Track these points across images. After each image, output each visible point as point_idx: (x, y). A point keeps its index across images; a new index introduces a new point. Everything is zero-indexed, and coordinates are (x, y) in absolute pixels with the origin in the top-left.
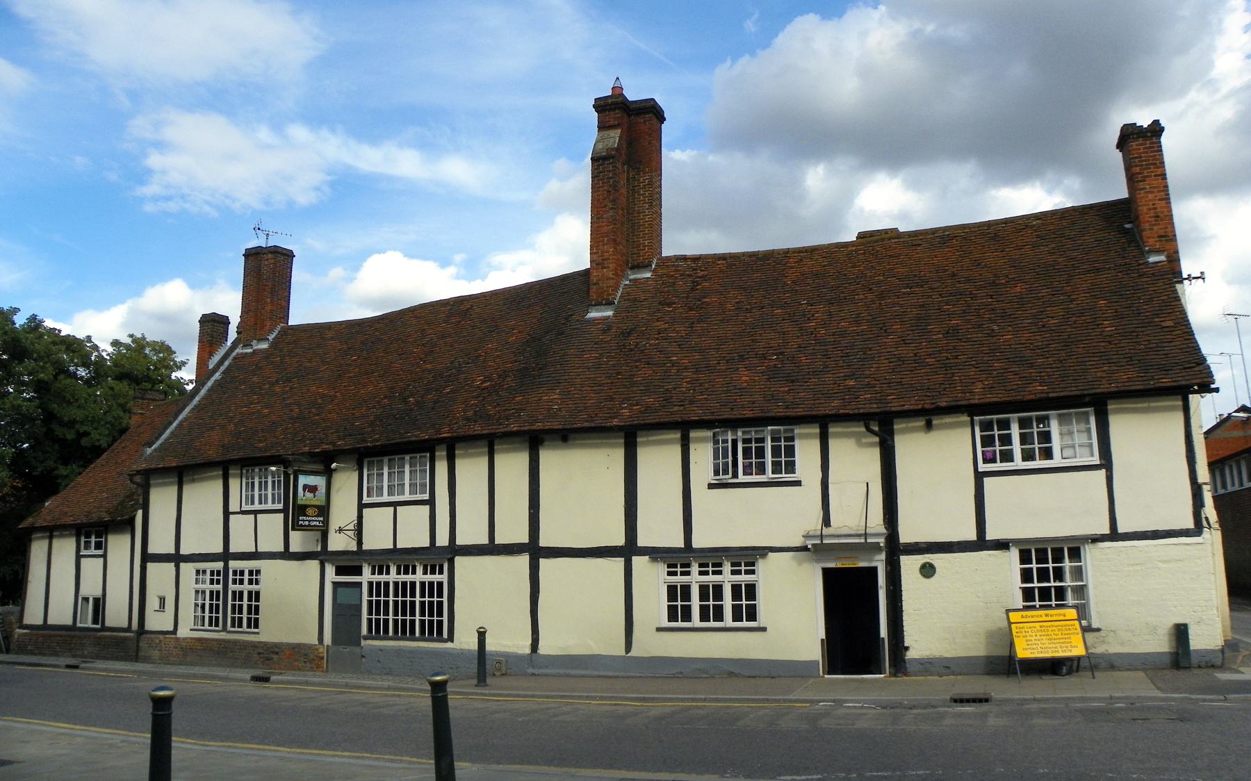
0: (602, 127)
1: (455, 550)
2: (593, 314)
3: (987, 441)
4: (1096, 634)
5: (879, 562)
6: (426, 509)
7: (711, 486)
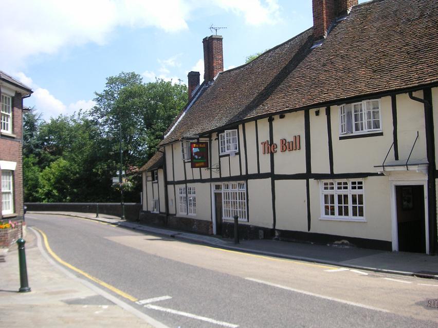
1: (248, 177)
7: (341, 138)
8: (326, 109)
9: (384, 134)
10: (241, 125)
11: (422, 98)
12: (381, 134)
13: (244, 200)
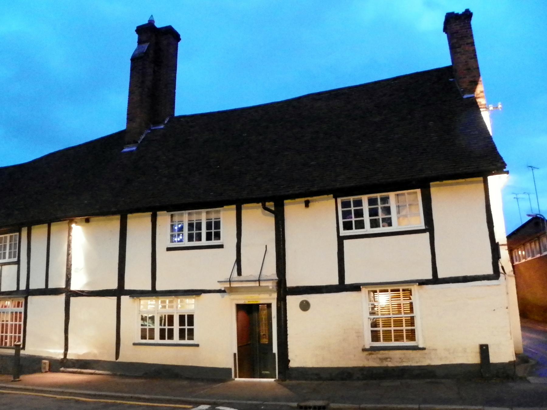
0: (140, 42)
1: (29, 292)
2: (126, 150)
3: (346, 214)
4: (420, 352)
5: (272, 299)
6: (16, 267)
7: (169, 249)
8: (152, 215)
9: (166, 249)
10: (26, 228)
11: (273, 209)
12: (221, 246)
13: (20, 321)
